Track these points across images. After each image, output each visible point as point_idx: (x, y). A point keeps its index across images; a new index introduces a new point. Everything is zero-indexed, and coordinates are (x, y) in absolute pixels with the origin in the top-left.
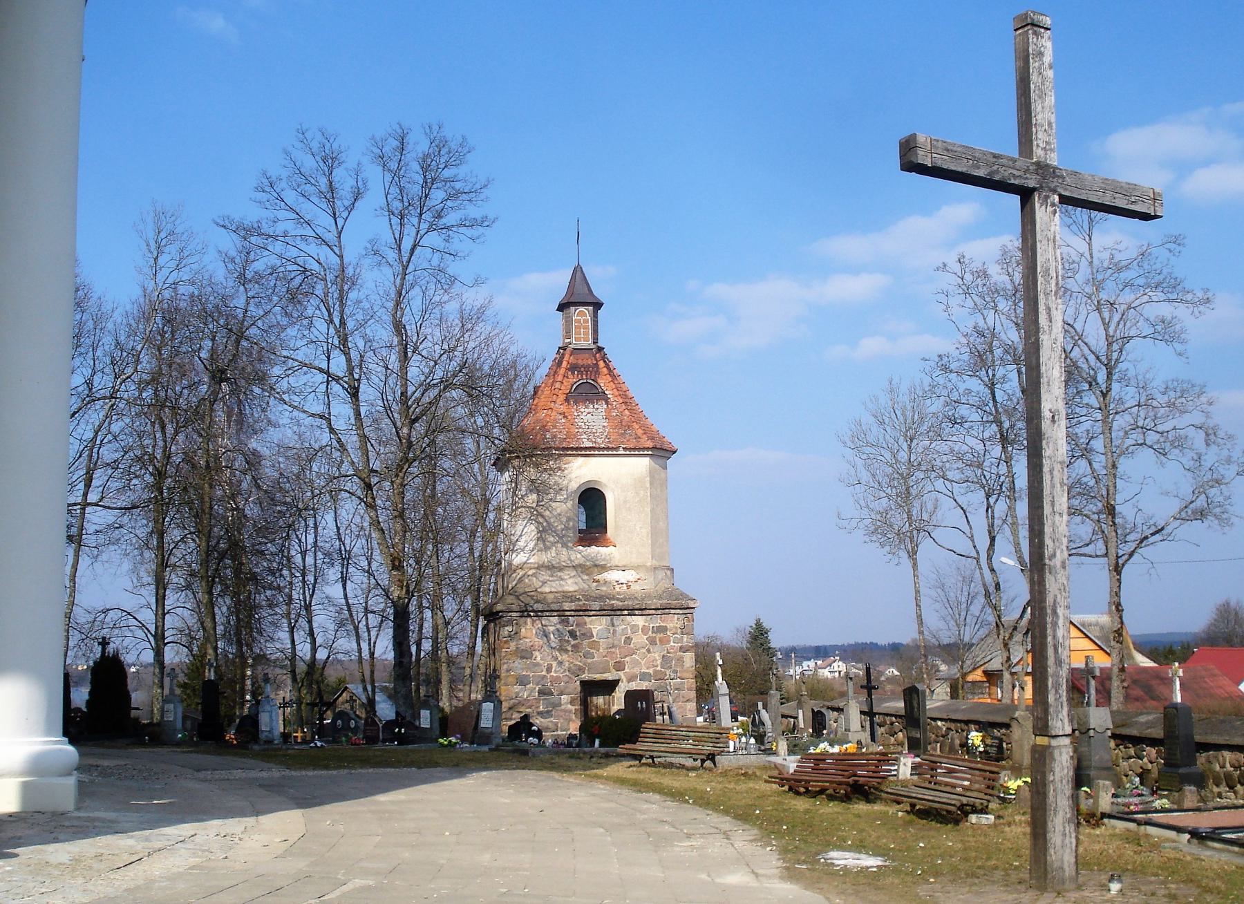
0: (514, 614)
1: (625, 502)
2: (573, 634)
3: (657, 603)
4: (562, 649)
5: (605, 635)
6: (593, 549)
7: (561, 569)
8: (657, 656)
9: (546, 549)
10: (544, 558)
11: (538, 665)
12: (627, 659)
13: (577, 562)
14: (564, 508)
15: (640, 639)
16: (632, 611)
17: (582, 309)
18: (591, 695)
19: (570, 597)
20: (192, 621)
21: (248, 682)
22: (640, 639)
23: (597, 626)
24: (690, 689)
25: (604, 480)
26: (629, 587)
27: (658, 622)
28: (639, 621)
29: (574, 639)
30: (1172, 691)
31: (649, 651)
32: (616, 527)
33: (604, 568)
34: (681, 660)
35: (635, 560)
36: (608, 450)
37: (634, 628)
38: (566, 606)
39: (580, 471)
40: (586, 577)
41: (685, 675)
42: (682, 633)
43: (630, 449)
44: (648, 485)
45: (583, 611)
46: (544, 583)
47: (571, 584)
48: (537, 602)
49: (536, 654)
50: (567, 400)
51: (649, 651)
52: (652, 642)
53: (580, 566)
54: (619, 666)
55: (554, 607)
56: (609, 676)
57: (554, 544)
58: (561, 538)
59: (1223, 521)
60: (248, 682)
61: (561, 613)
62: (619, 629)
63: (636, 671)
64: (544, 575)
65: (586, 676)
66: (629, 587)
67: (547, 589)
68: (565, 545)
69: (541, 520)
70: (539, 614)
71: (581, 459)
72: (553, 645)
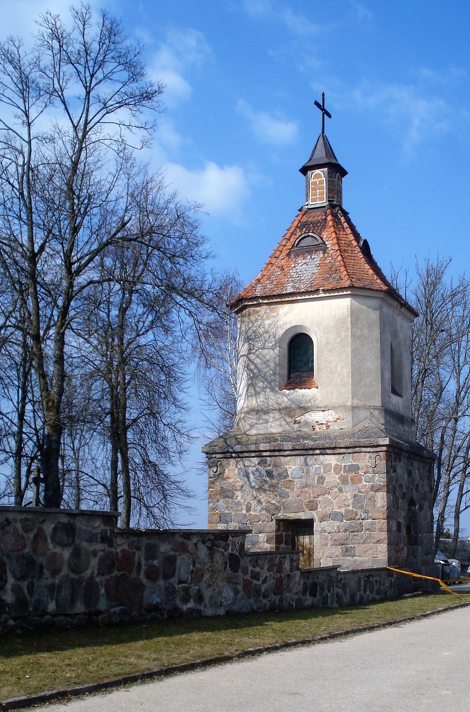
0: (218, 456)
1: (327, 343)
2: (269, 474)
3: (347, 442)
4: (260, 489)
5: (300, 474)
6: (300, 393)
7: (266, 412)
8: (348, 494)
9: (257, 394)
10: (254, 402)
11: (238, 504)
12: (320, 498)
13: (283, 405)
14: (273, 355)
15: (332, 478)
16: (323, 451)
17: (318, 171)
18: (298, 534)
19: (270, 438)
20: (168, 469)
21: (435, 526)
22: (332, 478)
23: (293, 466)
24: (381, 530)
25: (307, 324)
26: (328, 427)
27: (349, 460)
28: (332, 460)
29: (271, 481)
30: (449, 542)
31: (341, 490)
32: (318, 368)
33: (305, 410)
34: (372, 500)
35: (335, 400)
36: (310, 293)
37: (327, 467)
38: (262, 447)
39: (290, 317)
40: (289, 420)
41: (376, 515)
42: (374, 472)
43: (332, 290)
44: (349, 326)
45: (277, 451)
46: (252, 426)
47: (275, 426)
48: (239, 443)
49: (239, 494)
50: (288, 255)
51: (341, 490)
52: (344, 481)
53: (286, 408)
54: (313, 506)
55: (253, 448)
56: (303, 516)
57: (263, 389)
58: (269, 383)
59: (214, 257)
60: (435, 526)
61: (259, 453)
62: (312, 470)
63: (328, 510)
64: (252, 419)
65: (281, 515)
66: (328, 427)
67: (253, 432)
68: (272, 390)
69: (252, 367)
70: (239, 455)
71: (287, 307)
72: (253, 484)
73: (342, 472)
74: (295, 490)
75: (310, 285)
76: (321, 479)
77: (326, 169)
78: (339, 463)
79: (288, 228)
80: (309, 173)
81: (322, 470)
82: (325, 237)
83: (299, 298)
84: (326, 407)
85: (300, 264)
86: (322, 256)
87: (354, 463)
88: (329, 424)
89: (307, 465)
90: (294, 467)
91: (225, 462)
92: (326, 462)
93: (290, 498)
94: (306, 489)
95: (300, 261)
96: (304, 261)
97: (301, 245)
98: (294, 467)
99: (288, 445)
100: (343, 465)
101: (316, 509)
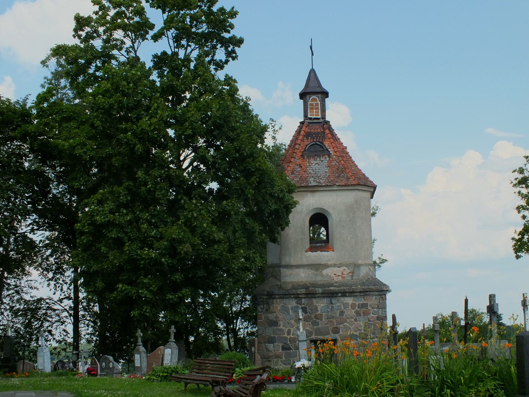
15: (350, 312)
16: (344, 294)
22: (350, 312)
23: (321, 304)
27: (362, 301)
28: (349, 300)
37: (346, 305)
50: (302, 156)
52: (358, 314)
54: (336, 330)
73: (357, 308)
74: (324, 320)
75: (327, 181)
76: (342, 313)
77: (320, 96)
78: (354, 302)
79: (44, 58)
80: (308, 97)
81: (343, 307)
82: (327, 145)
83: (320, 189)
84: (340, 264)
85: (313, 164)
86: (328, 159)
87: (365, 302)
88: (344, 276)
89: (332, 303)
90: (322, 305)
91: (271, 300)
92: (345, 302)
93: (320, 326)
94: (332, 320)
95: (312, 162)
96: (315, 162)
97: (310, 150)
98: (322, 305)
99: (320, 290)
100: (357, 303)
101: (339, 332)
